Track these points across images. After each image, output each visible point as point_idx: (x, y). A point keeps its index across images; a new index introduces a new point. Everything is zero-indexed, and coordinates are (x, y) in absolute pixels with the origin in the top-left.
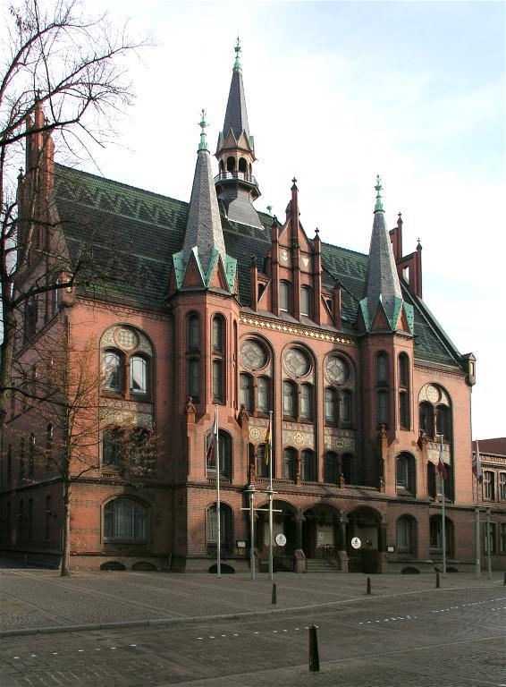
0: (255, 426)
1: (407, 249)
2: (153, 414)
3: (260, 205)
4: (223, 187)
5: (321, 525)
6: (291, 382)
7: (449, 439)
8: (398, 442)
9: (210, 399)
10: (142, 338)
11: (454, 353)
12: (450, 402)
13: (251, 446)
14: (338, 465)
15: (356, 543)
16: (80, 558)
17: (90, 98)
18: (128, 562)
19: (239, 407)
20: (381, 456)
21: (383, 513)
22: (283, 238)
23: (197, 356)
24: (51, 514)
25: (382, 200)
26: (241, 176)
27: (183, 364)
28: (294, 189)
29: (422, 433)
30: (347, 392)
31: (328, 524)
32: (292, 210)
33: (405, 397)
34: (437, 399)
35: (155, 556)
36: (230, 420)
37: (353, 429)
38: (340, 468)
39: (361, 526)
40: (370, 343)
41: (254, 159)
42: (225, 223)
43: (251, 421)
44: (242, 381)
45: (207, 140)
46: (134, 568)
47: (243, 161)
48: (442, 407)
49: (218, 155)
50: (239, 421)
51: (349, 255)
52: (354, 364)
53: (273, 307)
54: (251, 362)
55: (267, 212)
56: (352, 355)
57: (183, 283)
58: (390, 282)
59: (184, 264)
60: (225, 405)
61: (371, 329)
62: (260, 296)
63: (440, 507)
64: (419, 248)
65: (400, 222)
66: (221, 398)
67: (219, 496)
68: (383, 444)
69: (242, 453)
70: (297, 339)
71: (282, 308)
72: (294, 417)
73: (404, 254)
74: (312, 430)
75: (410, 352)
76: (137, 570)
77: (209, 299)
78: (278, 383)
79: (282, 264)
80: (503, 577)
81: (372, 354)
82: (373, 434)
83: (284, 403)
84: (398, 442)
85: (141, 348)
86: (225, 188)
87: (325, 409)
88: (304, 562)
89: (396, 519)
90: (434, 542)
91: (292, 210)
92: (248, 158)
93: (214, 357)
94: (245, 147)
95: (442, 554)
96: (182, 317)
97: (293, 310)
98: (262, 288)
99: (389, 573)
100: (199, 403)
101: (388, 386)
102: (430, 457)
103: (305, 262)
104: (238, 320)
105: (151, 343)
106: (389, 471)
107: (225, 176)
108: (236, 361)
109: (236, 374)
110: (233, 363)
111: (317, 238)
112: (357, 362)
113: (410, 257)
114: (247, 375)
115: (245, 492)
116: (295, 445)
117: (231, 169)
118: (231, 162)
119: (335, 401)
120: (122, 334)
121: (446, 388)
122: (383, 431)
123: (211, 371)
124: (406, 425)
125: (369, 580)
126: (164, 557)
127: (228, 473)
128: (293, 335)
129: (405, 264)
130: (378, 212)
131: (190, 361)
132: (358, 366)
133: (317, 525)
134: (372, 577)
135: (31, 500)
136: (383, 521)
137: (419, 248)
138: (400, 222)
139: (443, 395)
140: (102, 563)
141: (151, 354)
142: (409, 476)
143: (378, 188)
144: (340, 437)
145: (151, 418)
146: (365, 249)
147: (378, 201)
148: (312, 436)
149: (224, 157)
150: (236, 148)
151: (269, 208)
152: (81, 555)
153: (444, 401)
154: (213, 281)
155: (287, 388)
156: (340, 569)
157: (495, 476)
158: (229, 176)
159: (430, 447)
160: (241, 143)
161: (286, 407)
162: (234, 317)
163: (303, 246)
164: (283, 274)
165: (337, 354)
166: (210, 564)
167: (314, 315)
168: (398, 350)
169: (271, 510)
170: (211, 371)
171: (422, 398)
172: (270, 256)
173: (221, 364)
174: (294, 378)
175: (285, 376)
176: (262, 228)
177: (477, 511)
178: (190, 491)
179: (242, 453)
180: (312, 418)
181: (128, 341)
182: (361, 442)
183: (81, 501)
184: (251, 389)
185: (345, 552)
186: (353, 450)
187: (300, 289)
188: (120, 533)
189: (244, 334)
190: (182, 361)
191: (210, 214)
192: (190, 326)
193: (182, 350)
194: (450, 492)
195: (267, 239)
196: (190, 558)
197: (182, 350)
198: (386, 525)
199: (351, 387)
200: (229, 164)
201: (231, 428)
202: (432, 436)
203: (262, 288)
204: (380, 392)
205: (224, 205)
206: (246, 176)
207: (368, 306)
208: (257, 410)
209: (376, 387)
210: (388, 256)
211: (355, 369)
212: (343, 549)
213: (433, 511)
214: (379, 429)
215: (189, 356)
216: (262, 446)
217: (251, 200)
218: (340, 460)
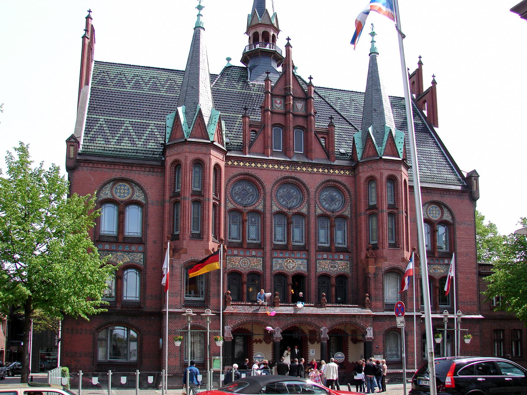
2: (144, 253)
12: (453, 218)
23: (179, 198)
25: (376, 45)
38: (438, 290)
40: (361, 170)
51: (155, 74)
52: (347, 190)
56: (346, 184)
61: (362, 159)
74: (304, 256)
75: (222, 164)
78: (268, 216)
81: (363, 180)
85: (135, 198)
112: (352, 190)
113: (428, 91)
120: (431, 209)
133: (309, 343)
138: (420, 64)
141: (451, 221)
143: (200, 8)
144: (333, 260)
146: (362, 87)
147: (199, 19)
149: (252, 32)
181: (436, 214)
211: (350, 196)
215: (173, 200)
218: (333, 281)
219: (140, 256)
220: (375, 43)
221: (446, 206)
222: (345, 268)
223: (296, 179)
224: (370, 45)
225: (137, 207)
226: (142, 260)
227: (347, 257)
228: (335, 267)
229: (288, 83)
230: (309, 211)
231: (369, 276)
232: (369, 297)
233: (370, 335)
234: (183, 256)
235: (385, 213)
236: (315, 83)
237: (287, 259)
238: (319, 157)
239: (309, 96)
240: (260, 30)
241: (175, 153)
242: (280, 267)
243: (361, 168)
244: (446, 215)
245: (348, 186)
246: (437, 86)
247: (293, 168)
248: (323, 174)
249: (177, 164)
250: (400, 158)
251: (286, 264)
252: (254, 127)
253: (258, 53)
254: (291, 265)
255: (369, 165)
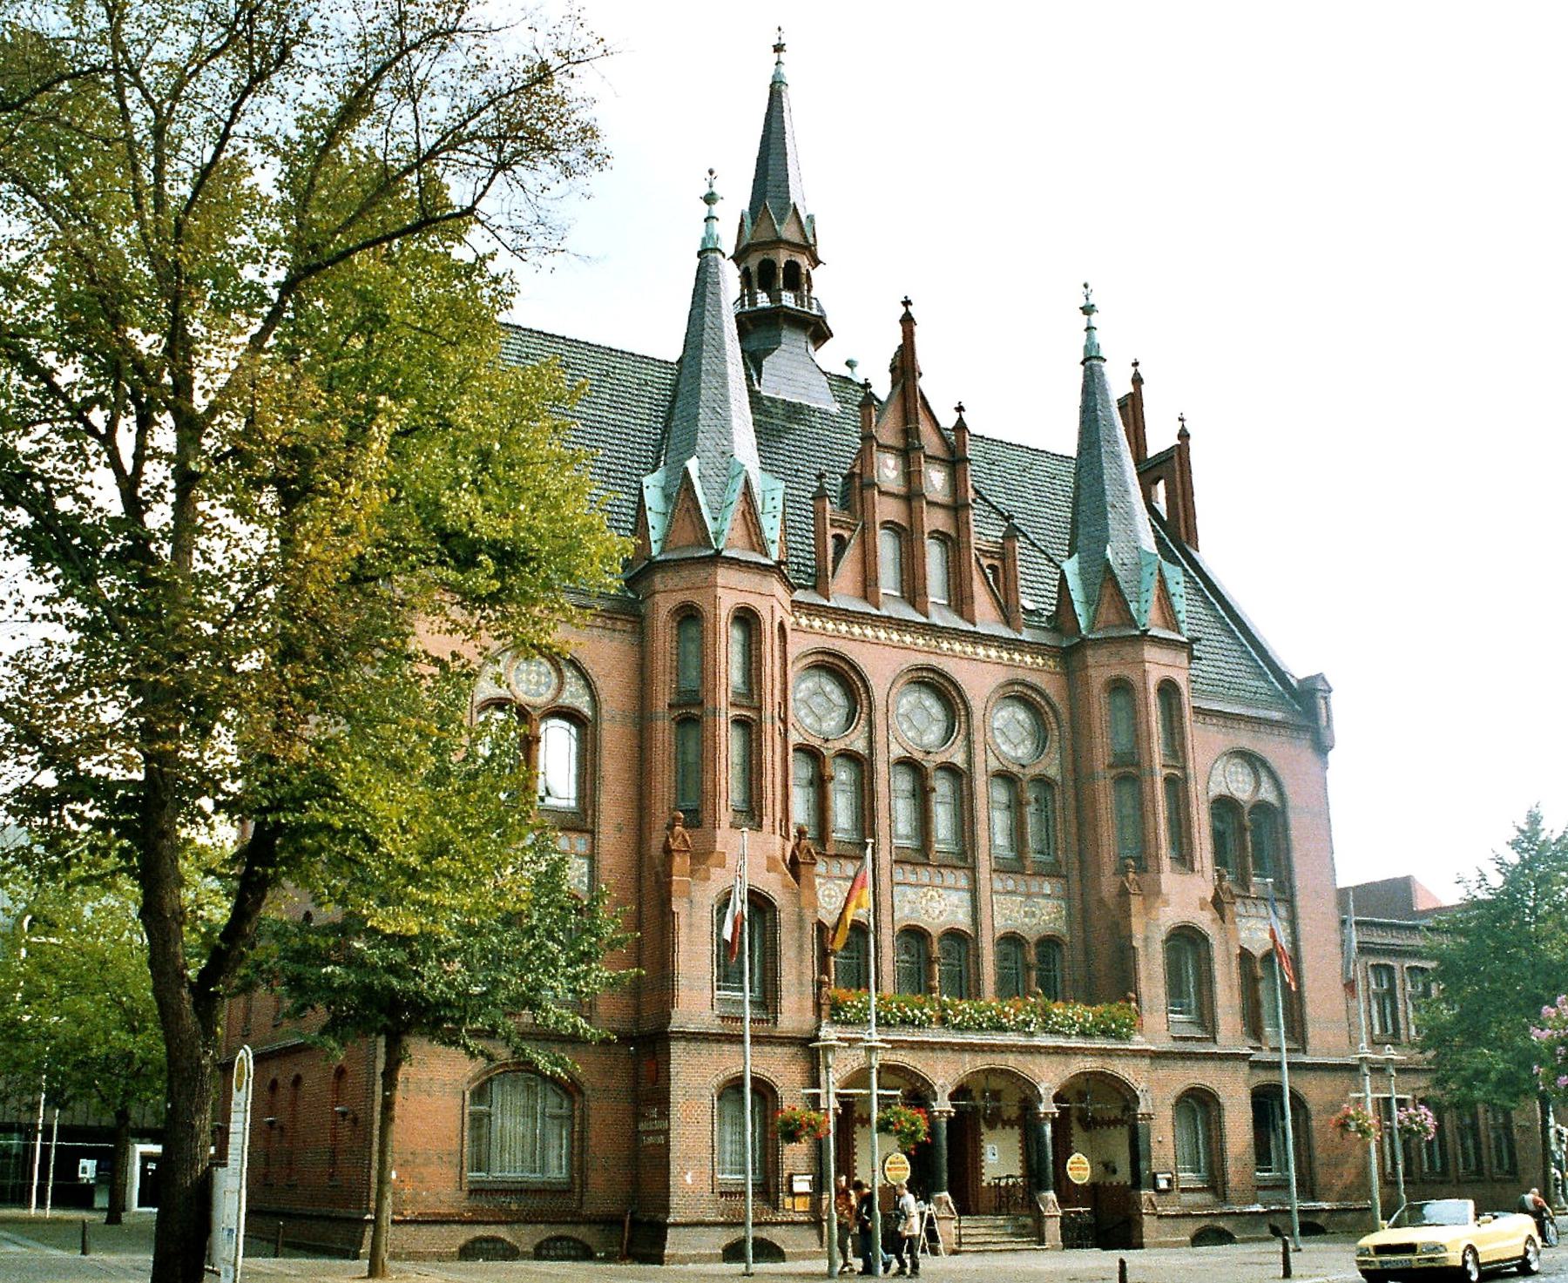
0: (829, 878)
1: (1159, 440)
3: (830, 357)
4: (748, 323)
5: (991, 1126)
6: (1006, 777)
7: (1285, 894)
8: (722, 865)
9: (725, 817)
10: (569, 674)
11: (1281, 675)
12: (1281, 794)
13: (821, 926)
14: (1028, 968)
15: (1079, 1169)
16: (411, 1229)
17: (501, 166)
18: (526, 1237)
19: (793, 832)
20: (1130, 937)
21: (1140, 1086)
22: (887, 431)
24: (344, 1114)
25: (1098, 337)
26: (788, 299)
27: (663, 730)
28: (907, 321)
29: (1221, 877)
30: (1042, 781)
31: (1008, 1123)
32: (904, 366)
33: (1177, 786)
34: (1249, 788)
35: (590, 1221)
36: (772, 866)
37: (1059, 876)
38: (1034, 974)
39: (1089, 1124)
40: (1090, 661)
41: (816, 262)
42: (756, 400)
43: (821, 868)
44: (800, 770)
45: (717, 227)
46: (540, 1254)
47: (792, 267)
48: (1261, 807)
49: (738, 258)
50: (794, 866)
53: (868, 586)
54: (820, 719)
55: (846, 372)
56: (1050, 691)
57: (665, 540)
58: (1129, 516)
59: (667, 497)
60: (760, 826)
61: (1091, 630)
62: (836, 562)
63: (1277, 1066)
64: (1184, 435)
65: (1137, 380)
66: (752, 813)
67: (751, 1062)
68: (1134, 910)
69: (801, 947)
70: (921, 659)
71: (888, 580)
72: (921, 853)
73: (1151, 453)
74: (963, 883)
75: (1181, 679)
76: (545, 1258)
77: (724, 576)
78: (881, 767)
79: (931, 497)
80: (152, 1250)
82: (1108, 885)
83: (898, 815)
84: (1166, 903)
85: (566, 699)
86: (755, 326)
87: (994, 829)
88: (954, 1223)
89: (1173, 1101)
90: (1262, 1154)
91: (904, 366)
92: (804, 262)
93: (733, 712)
94: (797, 239)
95: (743, 1193)
96: (1096, 692)
97: (912, 591)
98: (841, 543)
99: (1161, 1245)
100: (699, 825)
101: (1138, 765)
102: (1243, 935)
103: (936, 480)
104: (789, 622)
105: (589, 685)
106: (1149, 978)
107: (753, 302)
108: (784, 721)
109: (785, 748)
110: (778, 724)
111: (961, 426)
112: (1062, 708)
113: (1166, 457)
114: (811, 753)
115: (810, 1050)
116: (923, 922)
117: (767, 283)
118: (768, 269)
119: (1016, 806)
121: (1270, 760)
122: (1131, 875)
123: (730, 745)
124: (1184, 859)
125: (1122, 1263)
126: (609, 1222)
127: (768, 1000)
128: (919, 651)
129: (1155, 474)
130: (1091, 361)
131: (678, 724)
132: (1065, 716)
133: (984, 1129)
134: (1132, 1257)
135: (297, 1081)
136: (1142, 1109)
137: (1184, 435)
138: (1137, 380)
139: (1264, 778)
140: (461, 1242)
141: (587, 712)
142: (1199, 992)
143: (1088, 310)
145: (585, 869)
146: (672, 351)
147: (1089, 338)
148: (966, 896)
149: (753, 263)
150: (778, 242)
151: (850, 364)
152: (411, 1222)
153: (1267, 794)
154: (728, 534)
155: (904, 782)
156: (1041, 1241)
157: (1398, 975)
158: (763, 300)
159: (1241, 910)
160: (788, 232)
161: (1001, 840)
162: (779, 614)
163: (930, 442)
164: (887, 509)
165: (1021, 695)
166: (725, 1237)
167: (960, 600)
168: (1155, 675)
169: (875, 1091)
170: (730, 745)
171: (1215, 791)
172: (857, 470)
173: (749, 727)
174: (918, 756)
175: (897, 751)
176: (835, 408)
177: (1365, 1069)
178: (677, 1049)
179: (801, 947)
180: (964, 856)
182: (1082, 908)
183: (419, 1082)
184: (819, 784)
185: (1051, 1195)
186: (1061, 927)
187: (928, 542)
188: (509, 1167)
189: (899, 676)
190: (1102, 783)
191: (724, 385)
192: (680, 640)
193: (663, 697)
194: (1297, 1031)
195: (844, 431)
196: (676, 1225)
197: (663, 697)
198: (1150, 1117)
199: (1053, 772)
200: (759, 276)
201: (774, 885)
202: (1244, 883)
203: (841, 543)
204: (1121, 780)
205: (754, 361)
206: (799, 298)
207: (1083, 572)
208: (937, 846)
209: (1111, 766)
210: (1119, 456)
211: (1058, 722)
212: (1047, 1189)
213: (1264, 1077)
214: (1122, 870)
215: (1114, 772)
216: (1268, 957)
217: (811, 348)
218: (1032, 956)
219: (580, 867)
220: (1095, 332)
221: (1264, 763)
222: (1056, 919)
223: (843, 658)
224: (1082, 337)
225: (566, 725)
226: (586, 880)
227: (1059, 891)
228: (1033, 914)
229: (913, 417)
230: (970, 760)
231: (1134, 944)
232: (1137, 1001)
233: (1147, 1106)
234: (715, 872)
235: (723, 720)
236: (974, 426)
237: (925, 890)
238: (987, 619)
239: (959, 454)
240: (782, 257)
241: (682, 584)
242: (913, 911)
243: (1091, 656)
244: (573, 689)
245: (1055, 700)
246: (1191, 443)
247: (933, 643)
248: (1011, 665)
249: (689, 616)
250: (766, 555)
251: (924, 902)
252: (841, 527)
253: (778, 315)
254: (936, 907)
255: (1114, 649)
